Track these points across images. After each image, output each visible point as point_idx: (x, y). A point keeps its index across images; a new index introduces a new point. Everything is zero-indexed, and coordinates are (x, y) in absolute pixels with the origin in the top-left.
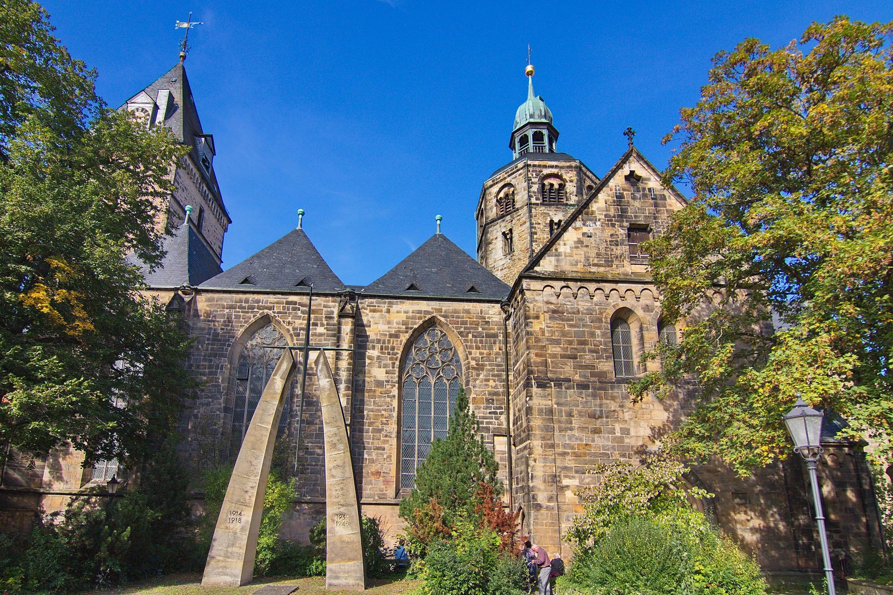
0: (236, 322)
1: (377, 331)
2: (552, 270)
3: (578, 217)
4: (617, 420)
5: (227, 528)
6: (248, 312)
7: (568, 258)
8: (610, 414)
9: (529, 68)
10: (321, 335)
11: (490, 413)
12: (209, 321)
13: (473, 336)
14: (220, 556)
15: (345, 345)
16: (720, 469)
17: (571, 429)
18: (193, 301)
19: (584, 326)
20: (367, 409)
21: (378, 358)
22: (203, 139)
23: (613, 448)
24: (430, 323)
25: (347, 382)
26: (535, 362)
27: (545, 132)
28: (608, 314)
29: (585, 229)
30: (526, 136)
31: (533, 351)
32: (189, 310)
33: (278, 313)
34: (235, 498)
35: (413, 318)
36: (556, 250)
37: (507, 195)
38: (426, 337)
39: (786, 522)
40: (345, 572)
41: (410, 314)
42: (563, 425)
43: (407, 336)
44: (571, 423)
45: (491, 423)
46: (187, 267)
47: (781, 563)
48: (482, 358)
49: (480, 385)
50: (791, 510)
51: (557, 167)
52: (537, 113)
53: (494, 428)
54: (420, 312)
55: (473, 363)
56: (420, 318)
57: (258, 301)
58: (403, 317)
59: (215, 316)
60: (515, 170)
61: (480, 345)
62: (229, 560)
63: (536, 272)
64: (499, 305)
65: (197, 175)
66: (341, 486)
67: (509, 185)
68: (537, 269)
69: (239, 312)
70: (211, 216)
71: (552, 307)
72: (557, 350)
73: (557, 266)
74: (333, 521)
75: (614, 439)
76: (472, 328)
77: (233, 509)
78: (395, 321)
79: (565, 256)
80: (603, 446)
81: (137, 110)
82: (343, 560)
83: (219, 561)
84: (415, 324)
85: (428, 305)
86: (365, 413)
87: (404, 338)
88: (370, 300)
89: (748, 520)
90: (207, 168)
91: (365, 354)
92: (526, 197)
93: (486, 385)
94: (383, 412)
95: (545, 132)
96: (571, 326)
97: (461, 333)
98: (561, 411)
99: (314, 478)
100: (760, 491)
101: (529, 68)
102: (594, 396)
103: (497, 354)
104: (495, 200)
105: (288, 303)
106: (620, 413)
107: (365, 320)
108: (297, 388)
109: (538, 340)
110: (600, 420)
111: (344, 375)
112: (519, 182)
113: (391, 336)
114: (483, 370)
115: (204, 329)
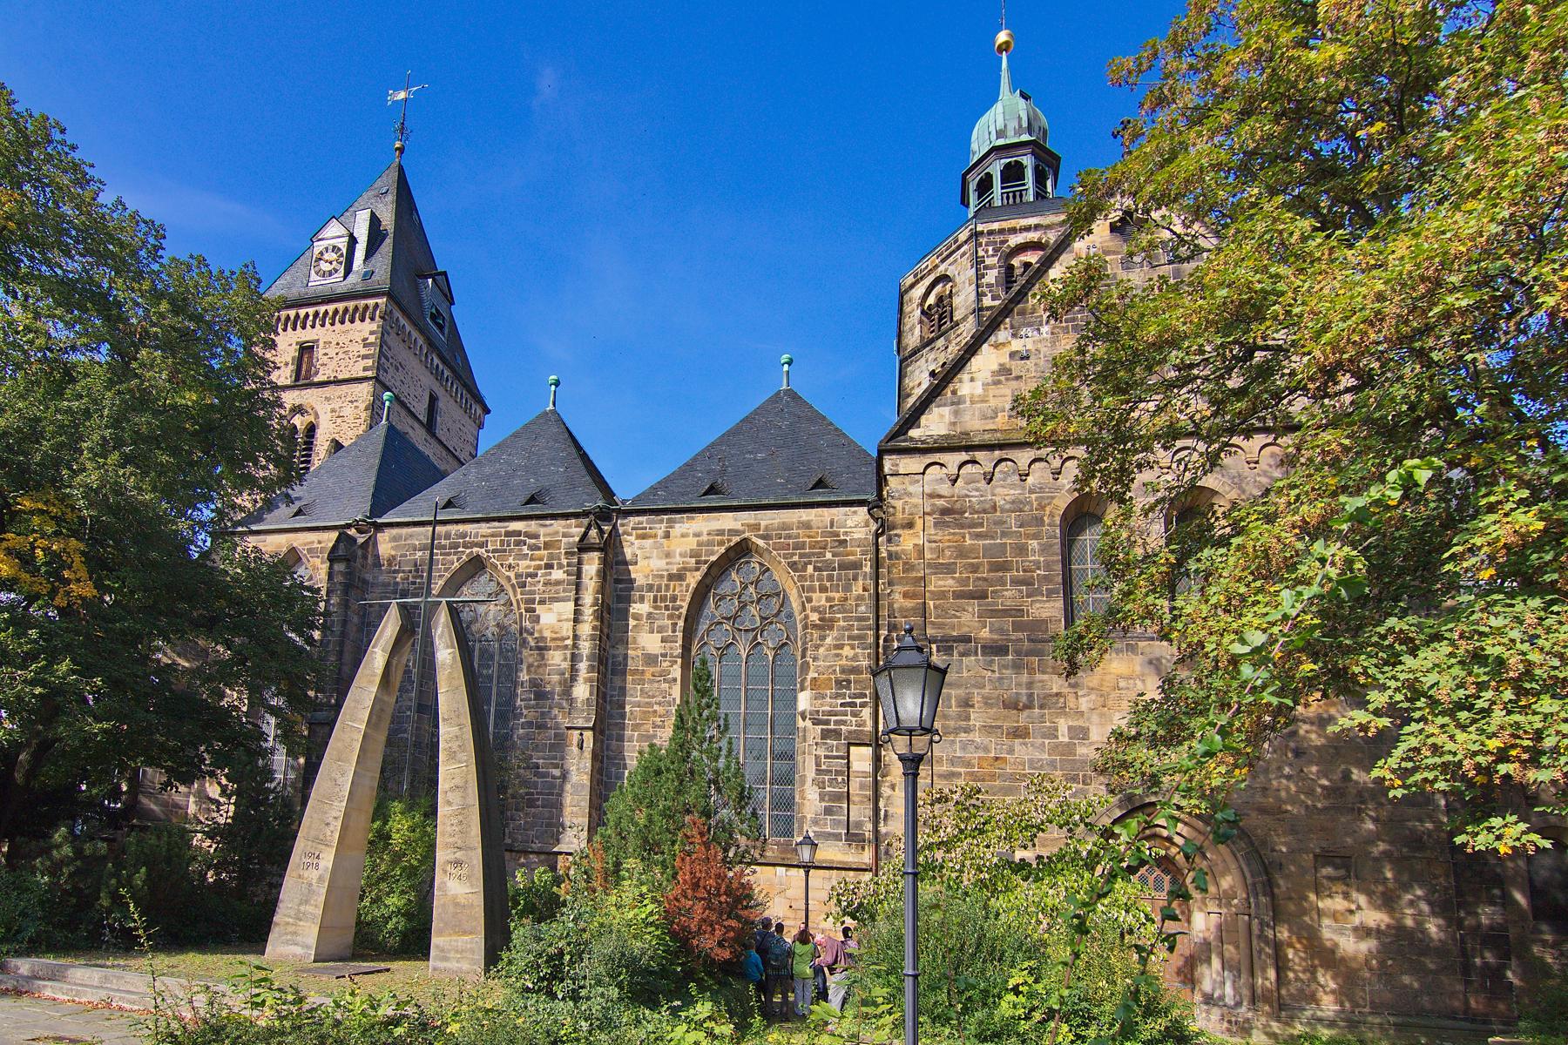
1: (647, 571)
2: (943, 432)
4: (1063, 711)
5: (300, 876)
6: (449, 554)
8: (1049, 701)
9: (1002, 37)
10: (558, 583)
11: (842, 705)
13: (815, 569)
15: (588, 598)
16: (1289, 808)
17: (967, 730)
18: (371, 543)
19: (1004, 534)
20: (631, 703)
21: (650, 615)
22: (430, 281)
23: (1052, 764)
24: (740, 551)
26: (901, 609)
27: (1028, 161)
29: (1016, 345)
30: (989, 176)
31: (898, 589)
32: (365, 557)
33: (494, 551)
34: (313, 833)
35: (710, 543)
36: (954, 392)
37: (940, 299)
38: (734, 575)
39: (1444, 918)
40: (457, 951)
41: (705, 538)
42: (952, 723)
43: (698, 575)
45: (844, 723)
46: (372, 490)
47: (1425, 1001)
49: (826, 656)
50: (1460, 893)
51: (1037, 227)
52: (1013, 124)
53: (850, 732)
54: (721, 532)
55: (814, 617)
56: (721, 543)
57: (464, 535)
58: (691, 543)
61: (828, 584)
63: (912, 439)
64: (866, 509)
65: (421, 341)
66: (460, 818)
67: (944, 278)
68: (914, 433)
71: (941, 503)
72: (948, 583)
73: (954, 424)
74: (445, 871)
75: (1055, 749)
76: (814, 554)
77: (309, 849)
78: (678, 551)
79: (972, 402)
80: (1031, 761)
81: (327, 249)
82: (456, 933)
84: (712, 553)
86: (628, 708)
87: (693, 580)
88: (637, 519)
89: (1351, 912)
90: (441, 328)
91: (627, 611)
92: (973, 296)
93: (837, 655)
94: (656, 707)
95: (1028, 161)
96: (978, 536)
97: (793, 565)
99: (547, 815)
100: (1384, 852)
101: (1002, 37)
102: (1017, 667)
105: (508, 534)
106: (1071, 698)
109: (909, 567)
110: (1026, 712)
111: (586, 647)
112: (961, 271)
113: (671, 577)
114: (831, 628)
115: (389, 584)
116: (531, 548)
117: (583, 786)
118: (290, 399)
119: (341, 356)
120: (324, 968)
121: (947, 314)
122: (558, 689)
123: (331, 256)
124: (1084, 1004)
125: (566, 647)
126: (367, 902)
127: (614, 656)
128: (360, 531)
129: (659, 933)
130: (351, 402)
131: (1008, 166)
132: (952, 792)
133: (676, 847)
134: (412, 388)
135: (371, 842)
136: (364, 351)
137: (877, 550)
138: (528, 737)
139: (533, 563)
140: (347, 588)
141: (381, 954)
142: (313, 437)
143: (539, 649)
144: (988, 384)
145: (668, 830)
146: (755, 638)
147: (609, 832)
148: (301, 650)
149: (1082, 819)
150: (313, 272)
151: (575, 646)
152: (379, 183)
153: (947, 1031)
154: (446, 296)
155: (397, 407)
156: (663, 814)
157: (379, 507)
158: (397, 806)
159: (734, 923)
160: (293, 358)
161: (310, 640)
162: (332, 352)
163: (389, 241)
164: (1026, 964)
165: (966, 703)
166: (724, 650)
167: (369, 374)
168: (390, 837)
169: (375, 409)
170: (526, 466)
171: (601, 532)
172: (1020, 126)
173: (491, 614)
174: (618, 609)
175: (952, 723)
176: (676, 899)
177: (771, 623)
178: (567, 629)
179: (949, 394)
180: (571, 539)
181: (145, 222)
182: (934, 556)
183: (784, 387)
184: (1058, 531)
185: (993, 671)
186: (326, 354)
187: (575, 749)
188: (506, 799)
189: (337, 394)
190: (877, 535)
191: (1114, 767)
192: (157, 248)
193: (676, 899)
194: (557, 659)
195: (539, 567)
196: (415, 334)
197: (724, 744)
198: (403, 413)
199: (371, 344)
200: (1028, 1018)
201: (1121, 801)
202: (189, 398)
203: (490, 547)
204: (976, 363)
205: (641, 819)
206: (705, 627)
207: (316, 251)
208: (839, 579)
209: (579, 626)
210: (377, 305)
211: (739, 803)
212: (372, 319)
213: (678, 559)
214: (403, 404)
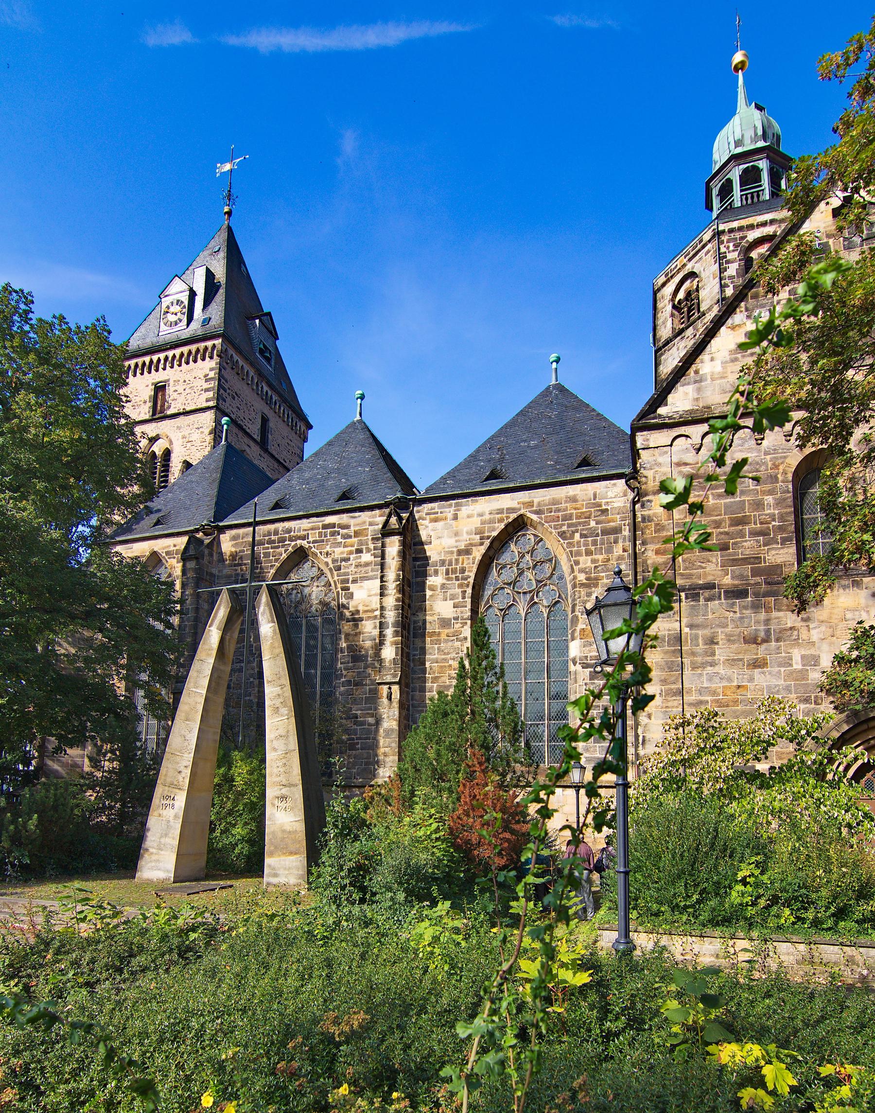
0: (266, 562)
3: (737, 306)
5: (160, 815)
6: (278, 547)
7: (718, 382)
9: (738, 57)
10: (367, 564)
12: (235, 565)
13: (582, 536)
14: (153, 848)
15: (392, 574)
17: (713, 664)
18: (217, 542)
21: (443, 586)
22: (257, 321)
23: (788, 689)
25: (396, 624)
28: (789, 466)
30: (729, 181)
31: (651, 547)
32: (211, 555)
33: (314, 542)
35: (491, 521)
36: (697, 372)
37: (689, 294)
38: (512, 546)
40: (285, 869)
41: (487, 517)
43: (483, 549)
44: (713, 654)
48: (596, 567)
54: (500, 511)
56: (501, 520)
57: (289, 531)
58: (476, 522)
59: (241, 558)
60: (699, 247)
61: (593, 548)
62: (162, 852)
64: (623, 481)
65: (252, 373)
66: (284, 761)
67: (692, 275)
68: (662, 411)
69: (268, 548)
70: (281, 426)
73: (697, 399)
74: (273, 805)
76: (580, 523)
77: (166, 793)
78: (465, 530)
79: (713, 380)
83: (152, 853)
84: (494, 530)
85: (513, 499)
86: (428, 664)
87: (478, 553)
88: (430, 505)
90: (268, 360)
91: (424, 583)
92: (717, 288)
94: (451, 662)
95: (763, 165)
97: (562, 535)
98: (696, 637)
99: (365, 755)
101: (738, 57)
102: (756, 607)
103: (620, 558)
104: (669, 308)
105: (325, 527)
107: (424, 535)
108: (340, 639)
110: (764, 646)
111: (391, 616)
113: (460, 552)
114: (596, 586)
115: (230, 576)
116: (346, 537)
117: (392, 730)
118: (151, 429)
119: (188, 391)
120: (179, 887)
121: (695, 306)
122: (370, 652)
123: (176, 308)
124: (804, 891)
125: (375, 617)
126: (217, 833)
127: (415, 622)
128: (206, 534)
129: (444, 846)
130: (198, 428)
131: (745, 171)
132: (693, 717)
133: (460, 775)
134: (247, 412)
135: (218, 785)
136: (206, 386)
137: (635, 516)
138: (349, 693)
139: (346, 549)
140: (199, 581)
141: (229, 874)
142: (169, 460)
143: (354, 620)
144: (726, 362)
145: (453, 762)
146: (532, 599)
147: (407, 766)
148: (158, 633)
149: (808, 733)
150: (162, 324)
151: (382, 616)
152: (212, 243)
153: (684, 918)
154: (271, 333)
155: (235, 430)
156: (449, 749)
157: (221, 511)
158: (236, 755)
159: (507, 835)
160: (150, 397)
161: (169, 625)
162: (180, 389)
163: (222, 291)
164: (753, 859)
165: (712, 641)
166: (505, 611)
167: (211, 404)
168: (233, 780)
169: (216, 432)
170: (338, 469)
171: (400, 519)
172: (756, 134)
173: (315, 593)
174: (417, 583)
175: (699, 659)
176: (459, 818)
177: (545, 585)
178: (375, 603)
179: (692, 374)
180: (376, 527)
181: (16, 292)
182: (682, 517)
183: (553, 382)
184: (790, 486)
185: (735, 612)
186: (175, 391)
187: (385, 701)
188: (331, 744)
189: (186, 423)
190: (634, 503)
191: (837, 687)
192: (27, 312)
193: (459, 818)
194: (369, 628)
195: (351, 553)
196: (247, 367)
197: (500, 688)
198: (240, 434)
199: (211, 379)
200: (754, 904)
201: (848, 716)
202: (62, 434)
203: (311, 539)
204: (715, 343)
205: (431, 754)
206: (490, 592)
207: (164, 305)
208: (602, 544)
209: (385, 599)
210: (214, 346)
211: (513, 736)
212: (211, 358)
213: (465, 536)
214: (240, 427)
